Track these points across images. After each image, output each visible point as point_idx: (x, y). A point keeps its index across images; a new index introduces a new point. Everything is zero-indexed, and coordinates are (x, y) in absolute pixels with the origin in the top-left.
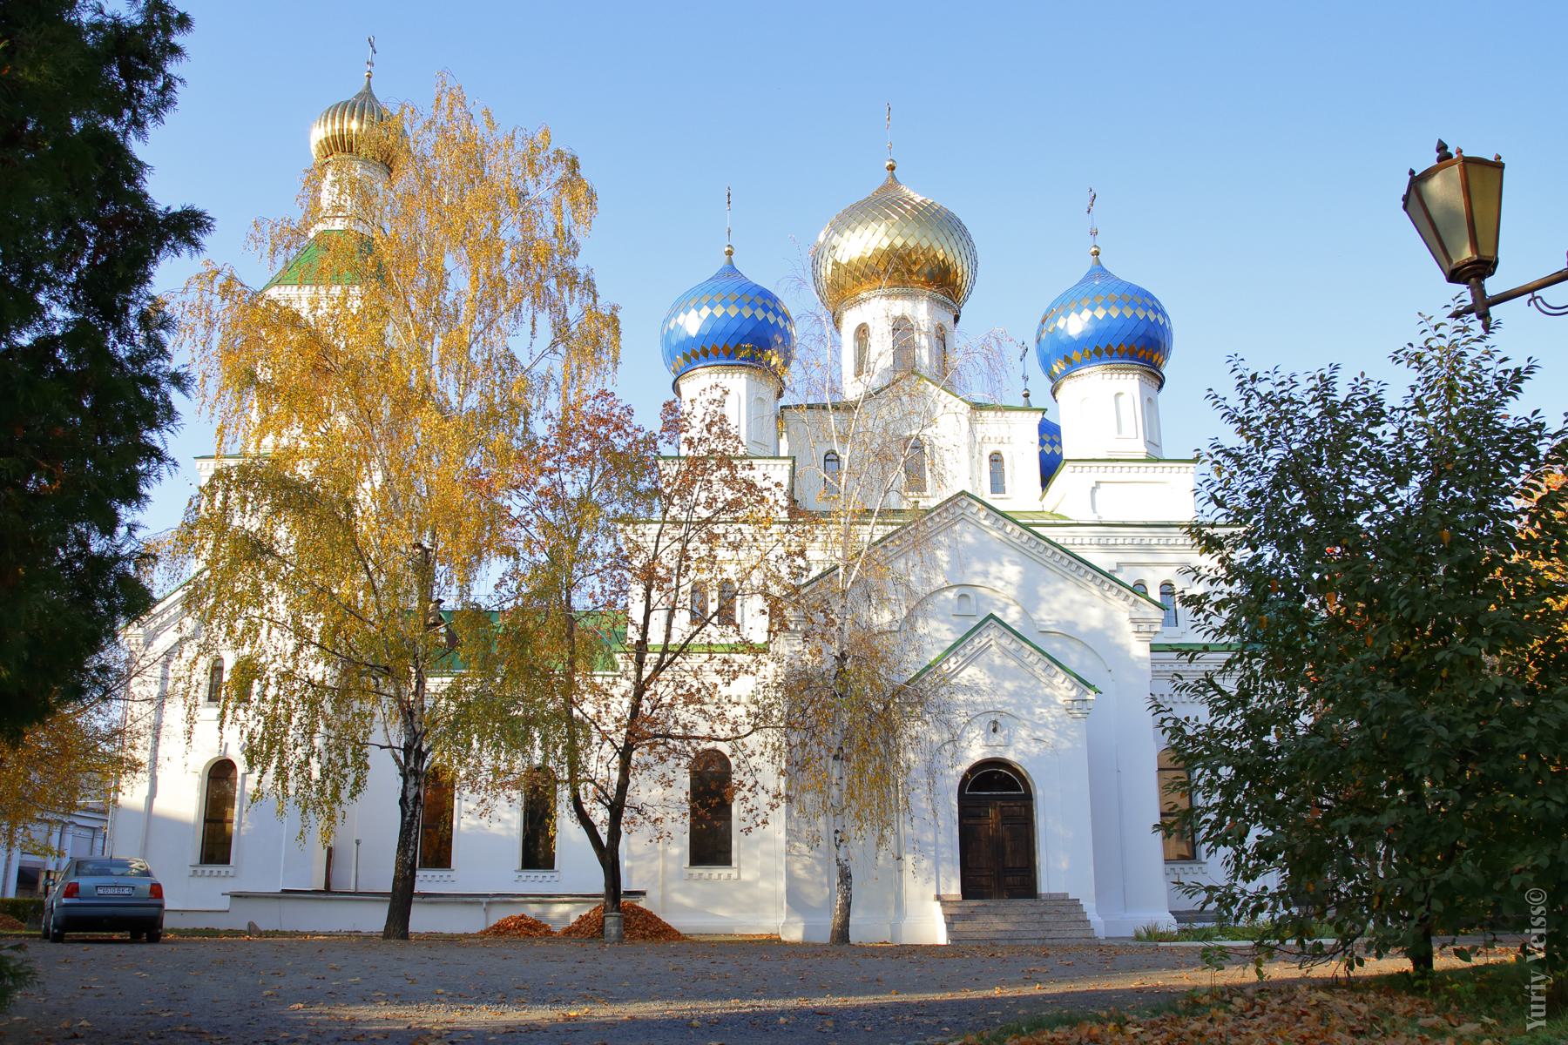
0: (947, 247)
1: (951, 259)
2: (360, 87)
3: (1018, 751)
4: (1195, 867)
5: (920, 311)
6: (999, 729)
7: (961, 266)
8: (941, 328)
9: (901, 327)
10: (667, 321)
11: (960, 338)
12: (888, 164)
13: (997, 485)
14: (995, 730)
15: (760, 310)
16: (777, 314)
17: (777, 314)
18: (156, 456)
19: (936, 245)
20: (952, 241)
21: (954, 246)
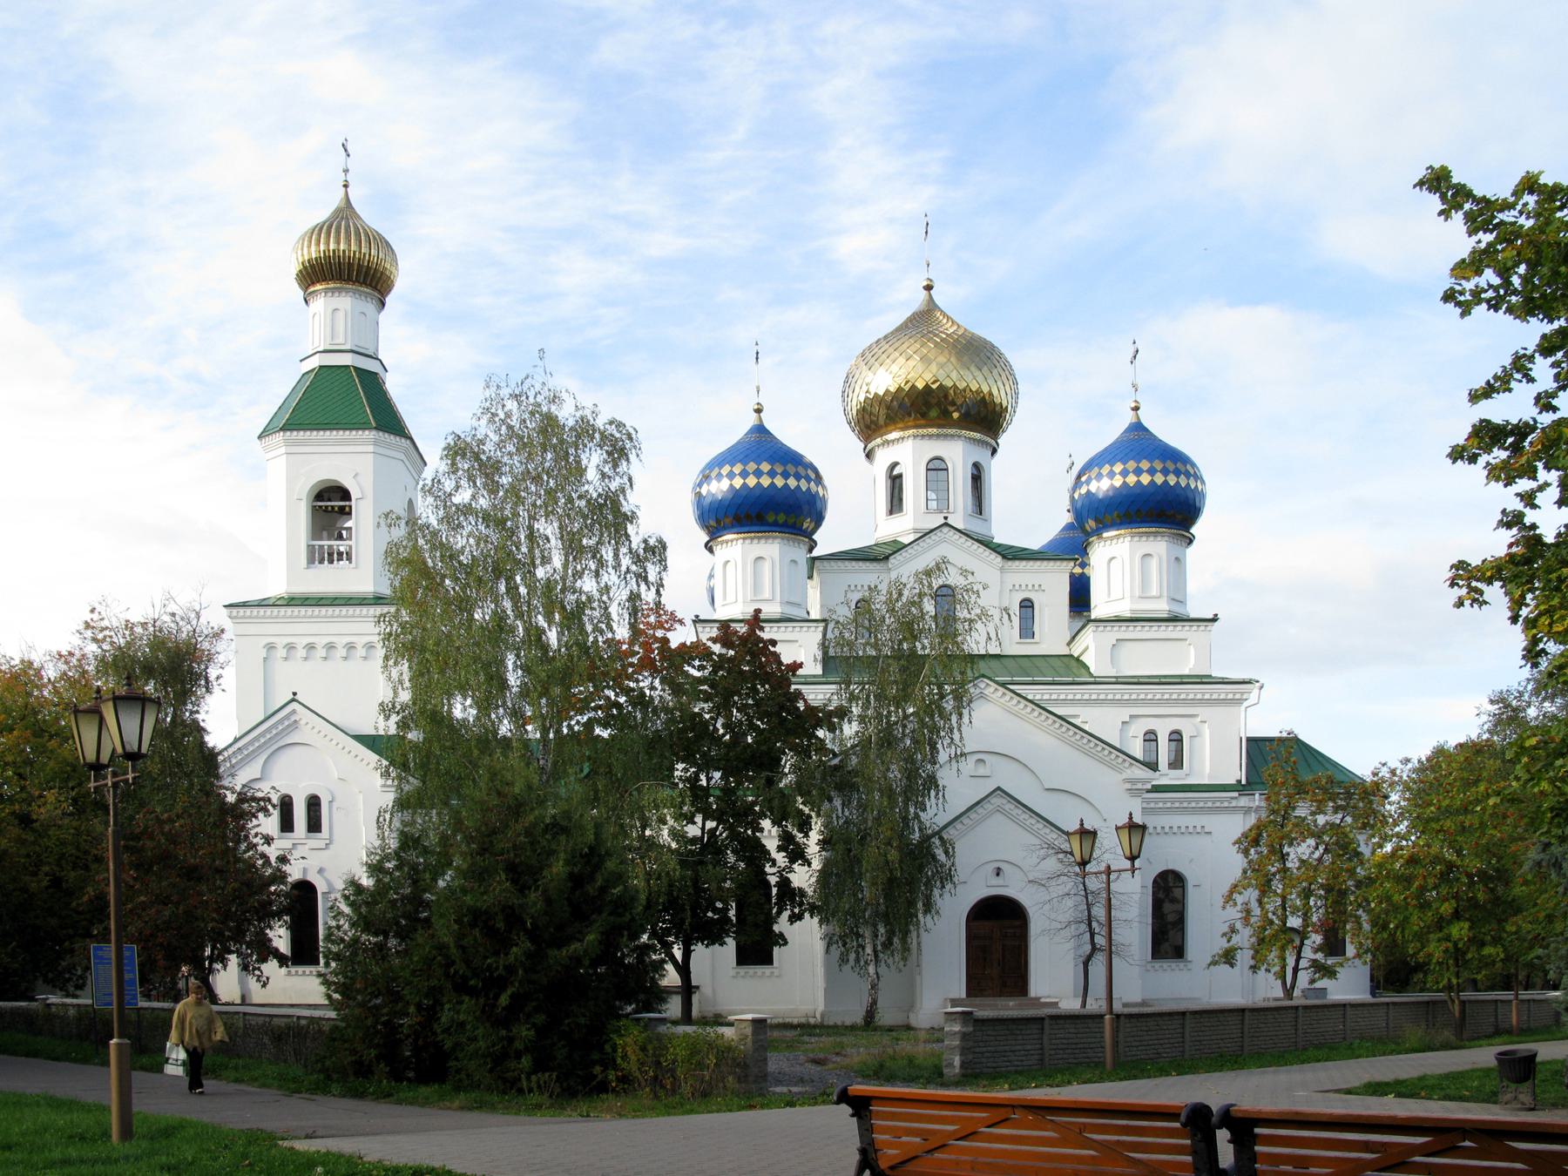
0: (991, 382)
1: (985, 389)
2: (334, 201)
3: (1013, 888)
4: (1182, 965)
5: (957, 452)
6: (1001, 874)
7: (1000, 395)
8: (976, 466)
9: (936, 467)
10: (700, 485)
11: (998, 471)
12: (925, 283)
13: (1027, 631)
14: (998, 875)
15: (1159, 474)
16: (1188, 475)
17: (1188, 475)
18: (818, 724)
19: (969, 378)
20: (973, 368)
21: (997, 377)
